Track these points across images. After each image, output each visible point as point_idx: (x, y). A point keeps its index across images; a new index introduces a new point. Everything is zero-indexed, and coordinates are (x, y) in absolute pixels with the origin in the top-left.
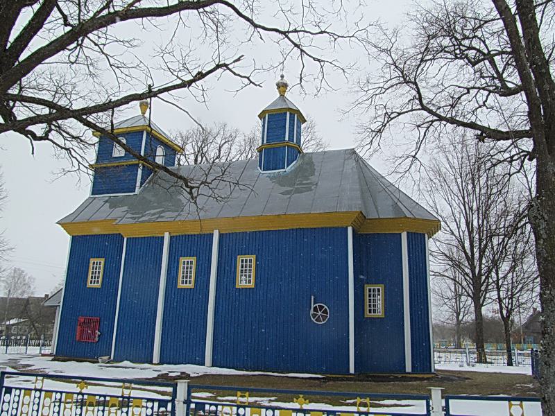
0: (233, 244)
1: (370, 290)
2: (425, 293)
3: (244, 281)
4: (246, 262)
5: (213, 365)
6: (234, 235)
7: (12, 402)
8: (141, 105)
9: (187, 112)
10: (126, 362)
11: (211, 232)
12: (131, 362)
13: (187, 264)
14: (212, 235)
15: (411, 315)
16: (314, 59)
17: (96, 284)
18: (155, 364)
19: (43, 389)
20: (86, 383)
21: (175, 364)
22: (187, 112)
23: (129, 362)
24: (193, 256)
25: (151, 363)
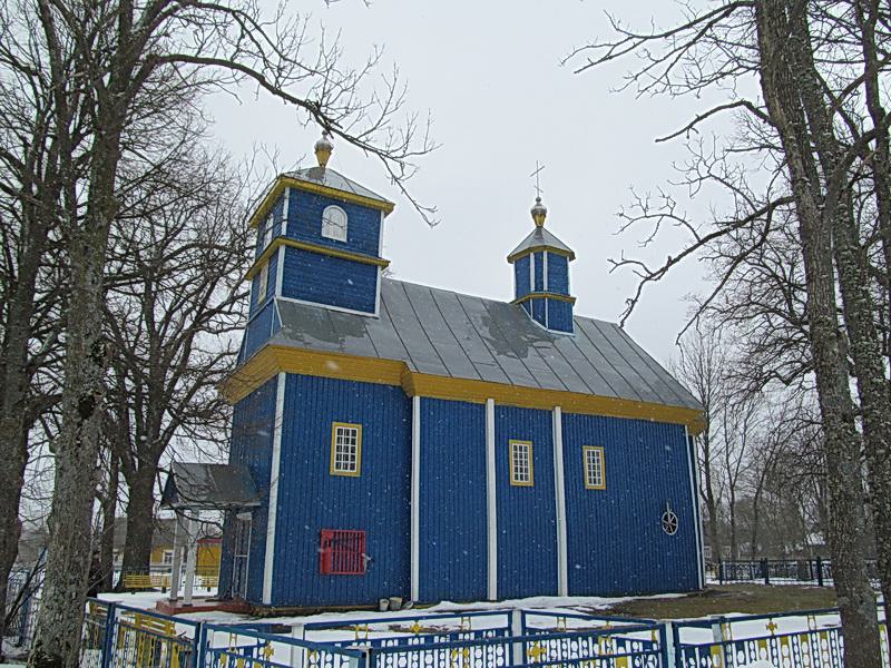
0: (582, 428)
1: (352, 467)
2: (327, 465)
3: (596, 479)
4: (521, 450)
5: (570, 594)
6: (337, 383)
7: (323, 662)
8: (321, 178)
9: (640, 288)
10: (443, 602)
11: (550, 409)
12: (452, 601)
13: (521, 450)
14: (483, 407)
15: (567, 519)
16: (218, 8)
17: (349, 470)
18: (493, 601)
19: (472, 628)
20: (413, 632)
21: (520, 598)
22: (640, 288)
23: (448, 603)
24: (357, 423)
25: (485, 599)
